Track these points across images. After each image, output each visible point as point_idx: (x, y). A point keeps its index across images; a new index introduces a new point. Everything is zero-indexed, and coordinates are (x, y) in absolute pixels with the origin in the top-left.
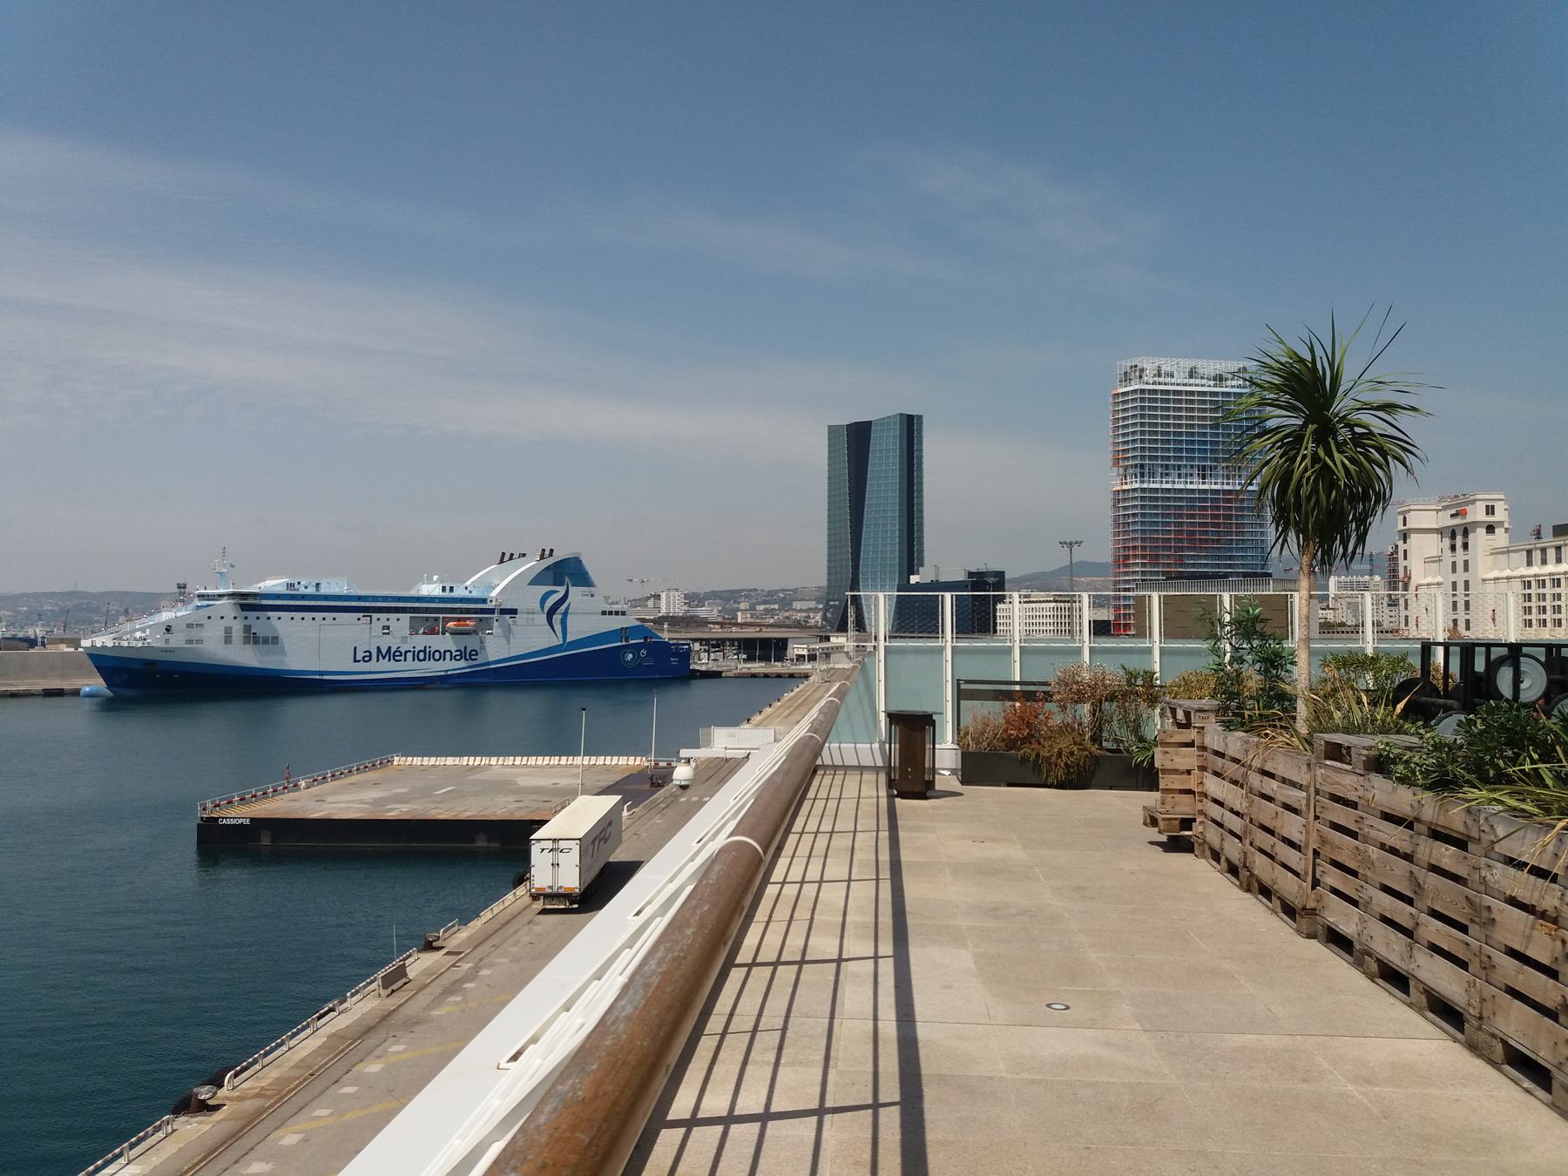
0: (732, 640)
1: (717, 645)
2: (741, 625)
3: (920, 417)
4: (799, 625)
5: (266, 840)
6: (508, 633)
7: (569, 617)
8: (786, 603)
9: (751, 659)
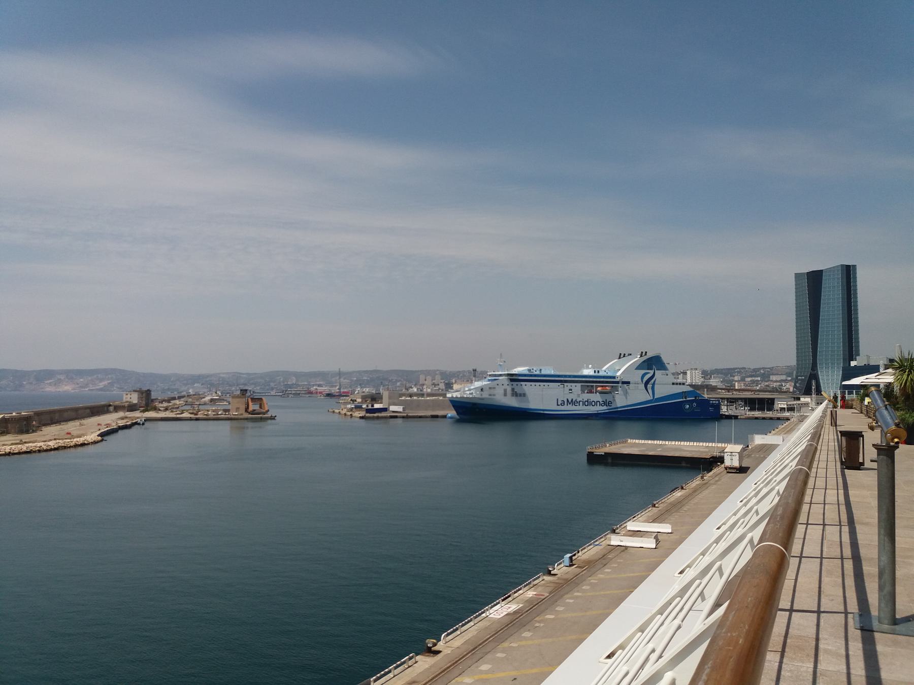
0: (741, 399)
1: (732, 401)
2: (739, 390)
3: (854, 266)
4: (778, 390)
5: (610, 461)
6: (626, 393)
7: (656, 386)
8: (766, 376)
9: (752, 409)
